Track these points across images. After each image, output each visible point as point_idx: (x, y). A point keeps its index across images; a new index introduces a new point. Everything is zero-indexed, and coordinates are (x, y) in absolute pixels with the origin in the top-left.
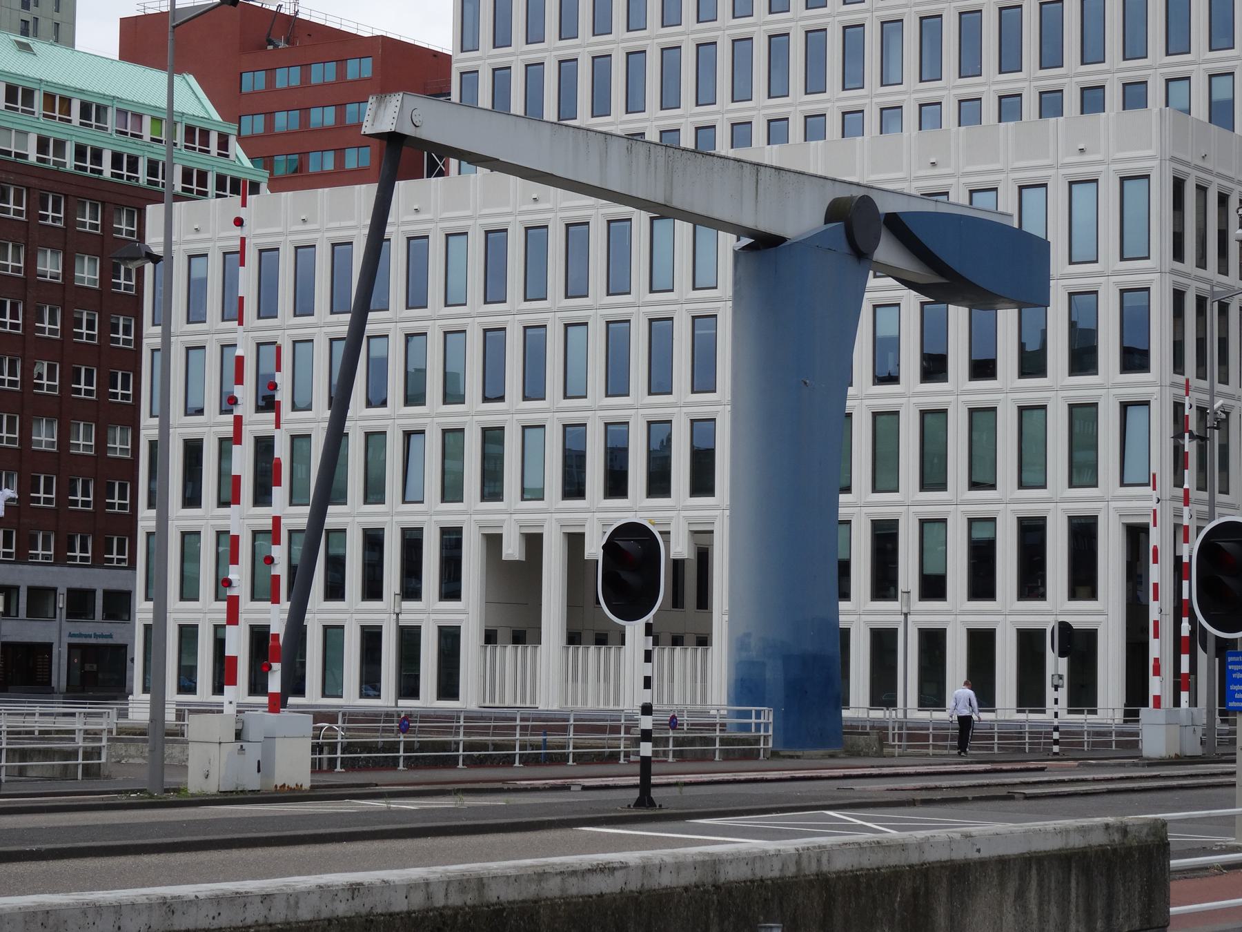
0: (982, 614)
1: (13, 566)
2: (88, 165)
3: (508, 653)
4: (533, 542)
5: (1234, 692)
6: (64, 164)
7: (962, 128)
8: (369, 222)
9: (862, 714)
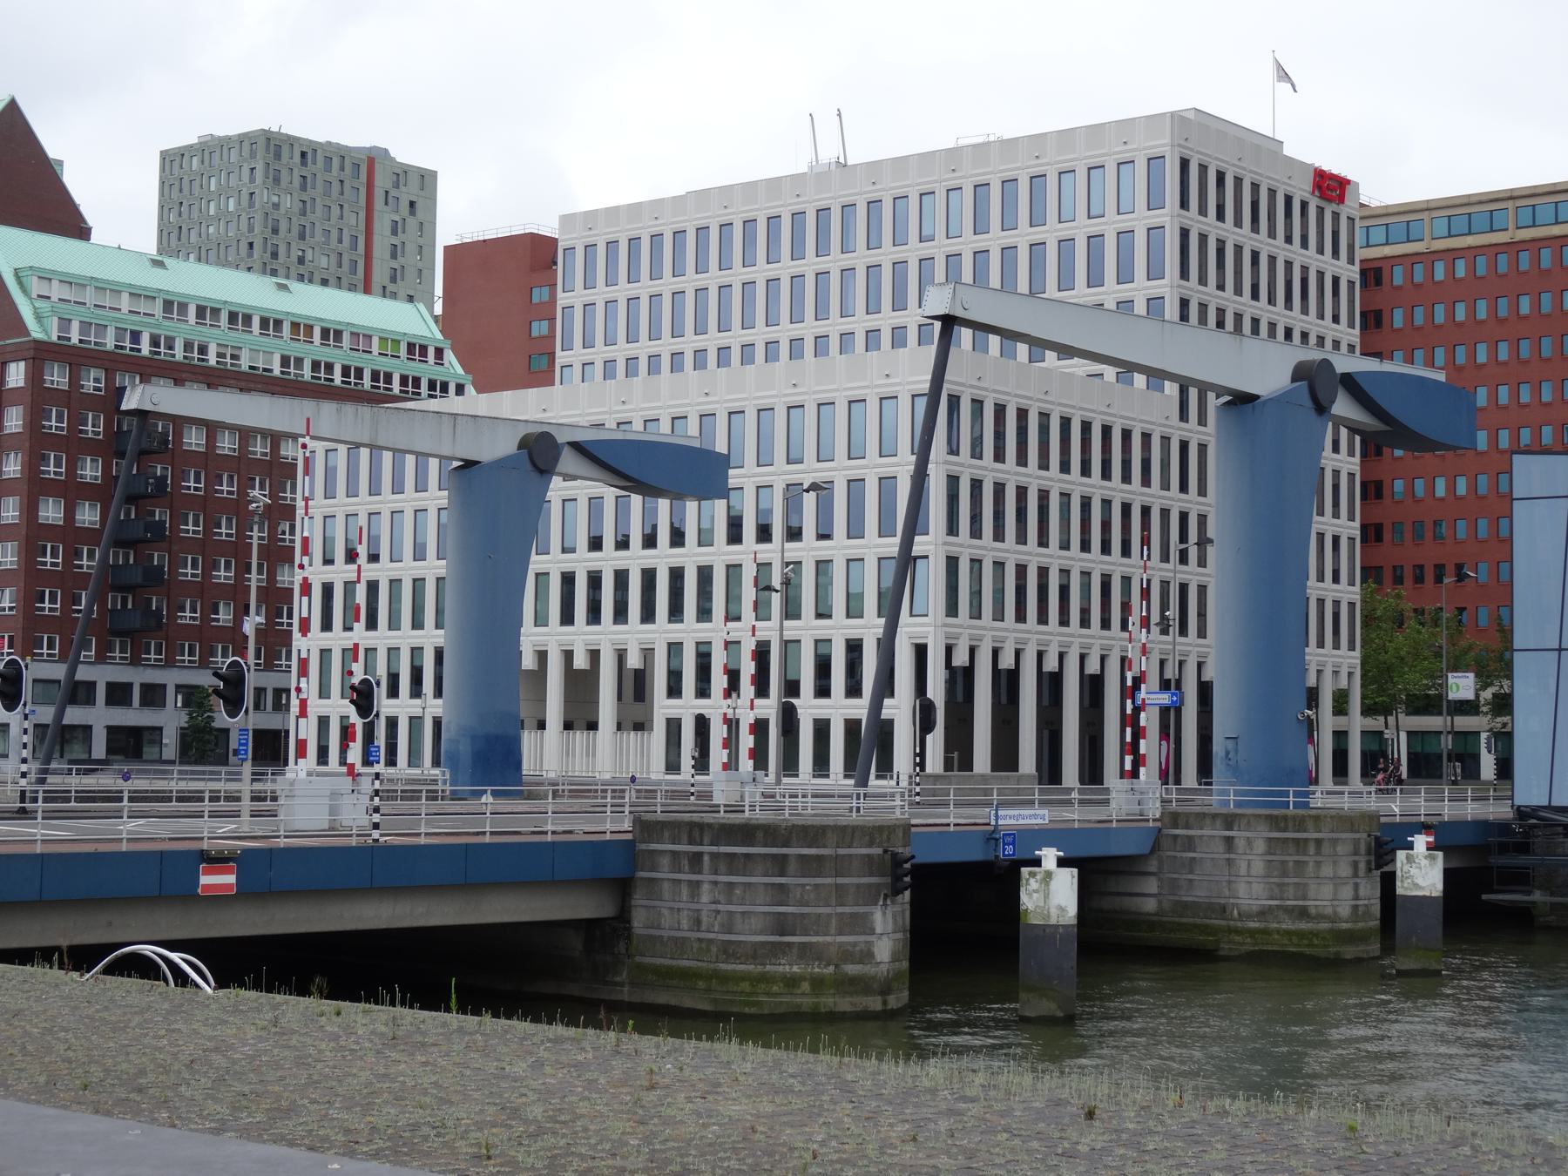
1: (261, 673)
2: (322, 375)
3: (579, 736)
4: (594, 655)
6: (303, 376)
7: (586, 384)
9: (661, 776)
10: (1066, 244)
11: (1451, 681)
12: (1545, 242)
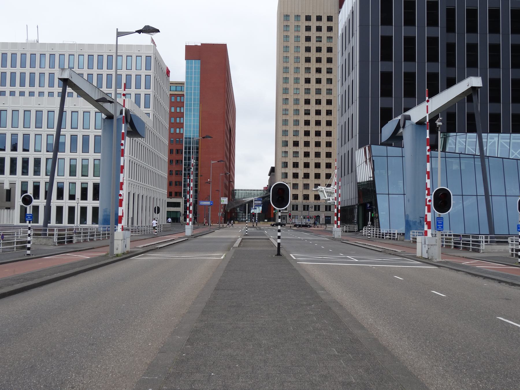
0: (83, 203)
5: (28, 216)
8: (59, 106)
10: (42, 74)
11: (222, 199)
12: (173, 95)
